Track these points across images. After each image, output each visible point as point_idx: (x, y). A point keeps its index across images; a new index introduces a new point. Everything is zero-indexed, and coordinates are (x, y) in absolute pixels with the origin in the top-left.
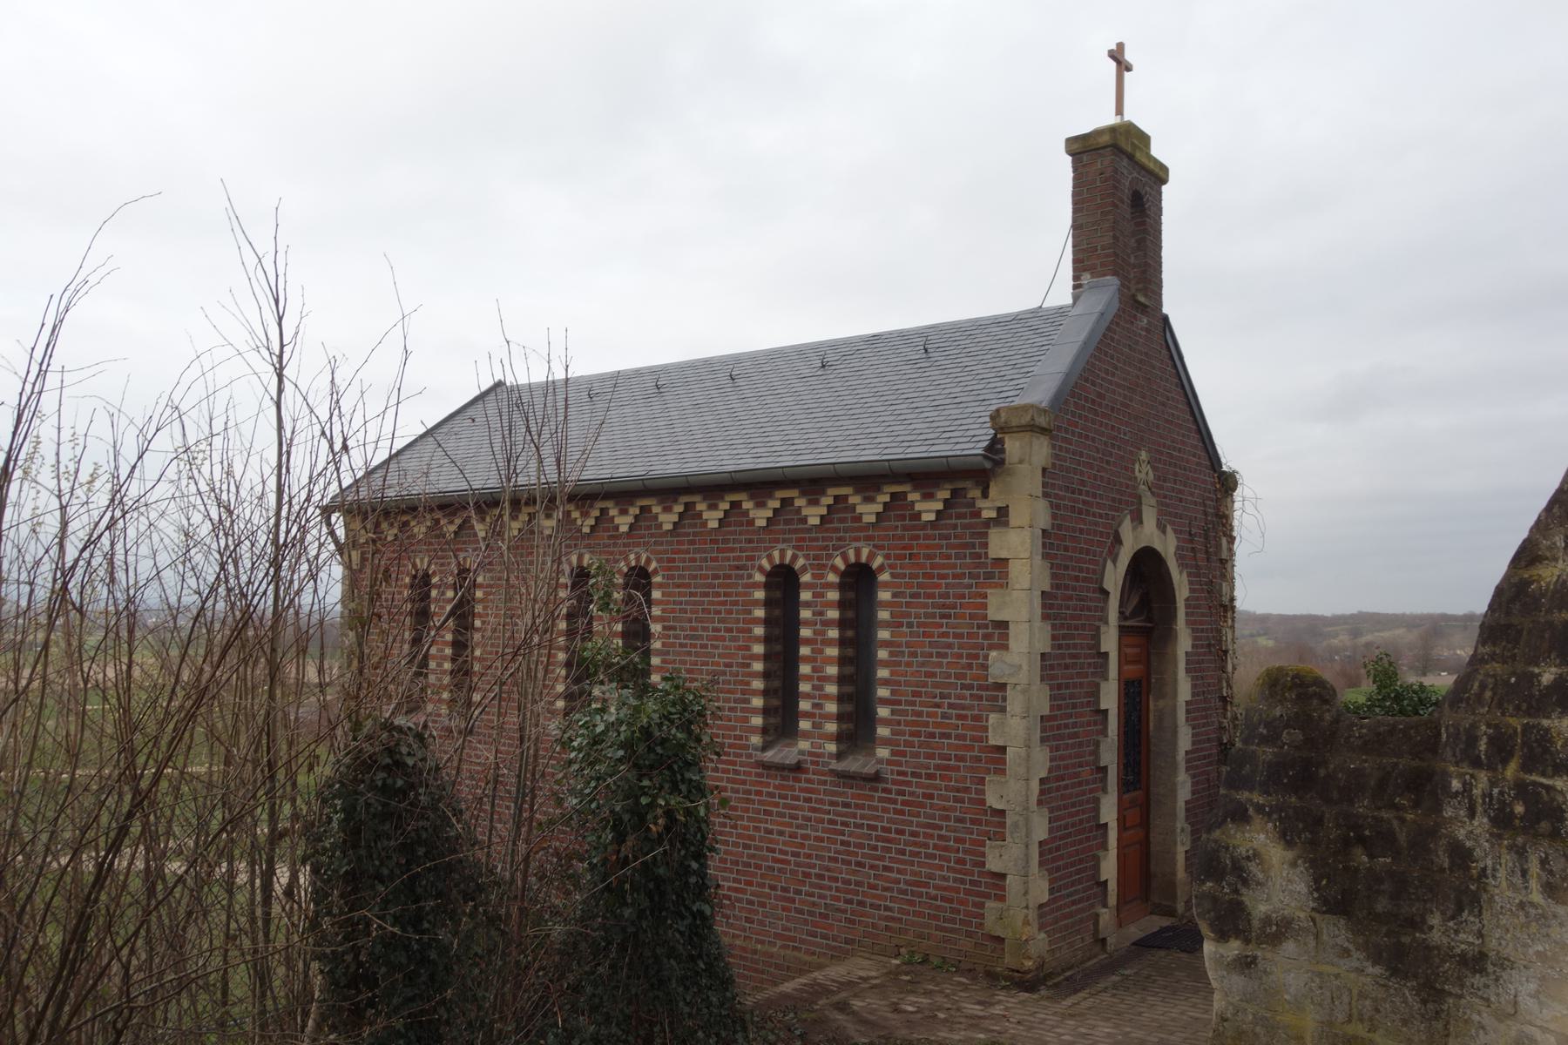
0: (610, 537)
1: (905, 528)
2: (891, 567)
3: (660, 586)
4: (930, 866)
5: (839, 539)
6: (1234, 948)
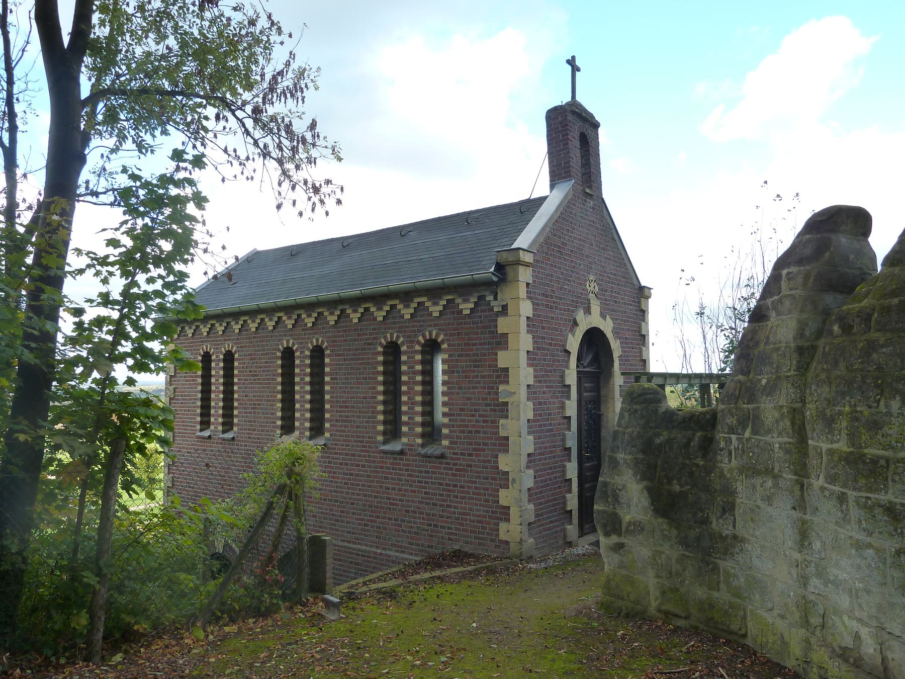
0: (303, 330)
1: (454, 319)
2: (448, 340)
3: (329, 356)
4: (471, 504)
5: (421, 326)
6: (614, 539)
